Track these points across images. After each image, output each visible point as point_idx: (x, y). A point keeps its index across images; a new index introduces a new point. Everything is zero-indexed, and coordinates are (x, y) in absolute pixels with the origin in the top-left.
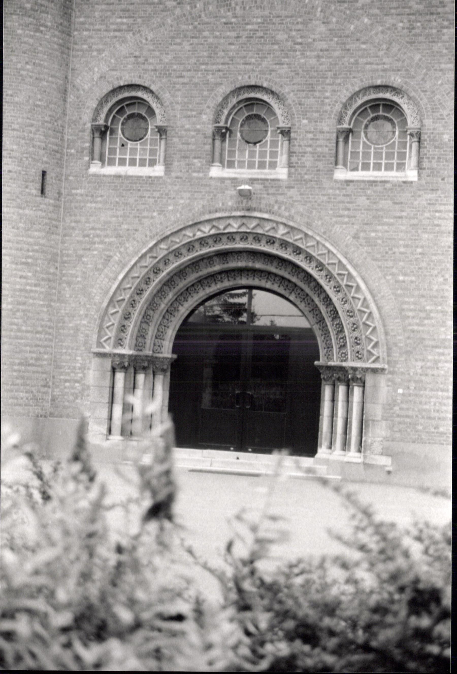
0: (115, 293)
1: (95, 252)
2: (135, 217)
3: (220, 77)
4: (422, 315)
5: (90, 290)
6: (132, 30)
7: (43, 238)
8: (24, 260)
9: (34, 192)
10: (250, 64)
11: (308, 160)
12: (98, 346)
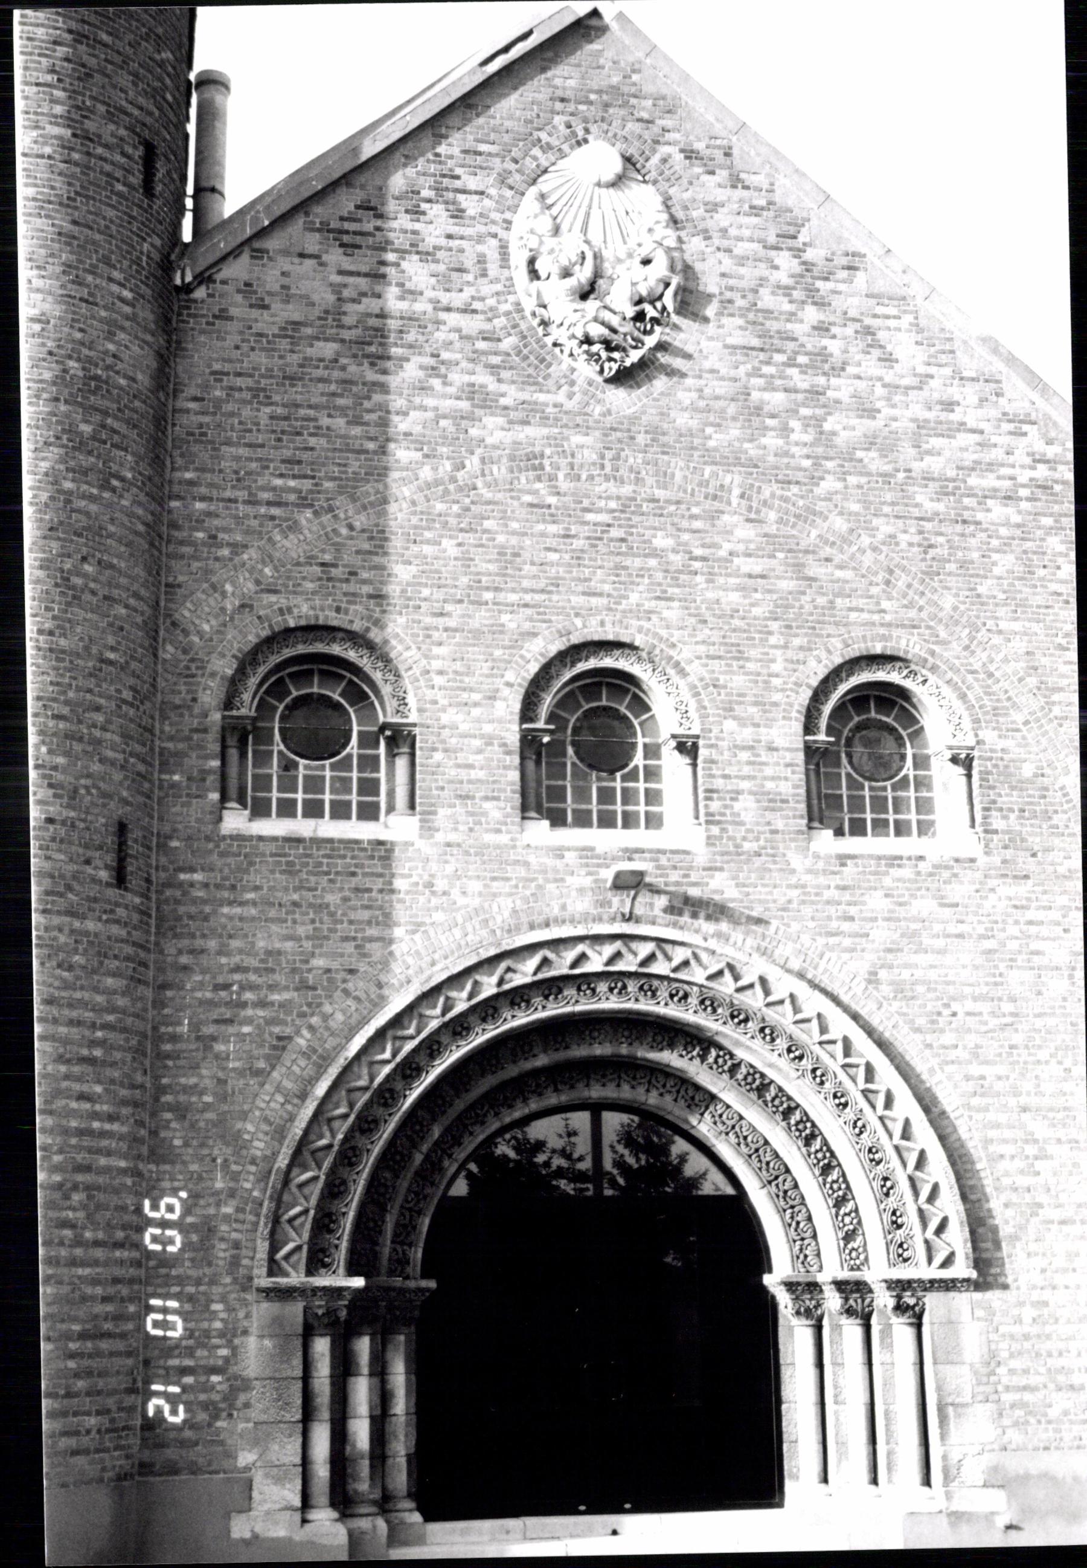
0: (307, 1132)
1: (246, 1029)
2: (346, 939)
3: (531, 620)
4: (1031, 1150)
5: (239, 1125)
6: (311, 506)
7: (123, 994)
8: (85, 1052)
9: (104, 875)
10: (601, 595)
11: (747, 808)
12: (271, 1273)
